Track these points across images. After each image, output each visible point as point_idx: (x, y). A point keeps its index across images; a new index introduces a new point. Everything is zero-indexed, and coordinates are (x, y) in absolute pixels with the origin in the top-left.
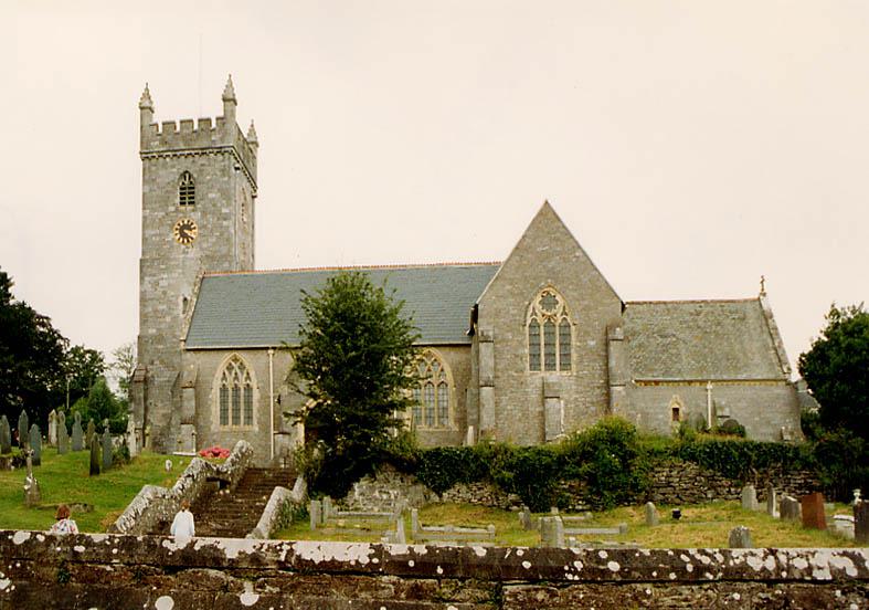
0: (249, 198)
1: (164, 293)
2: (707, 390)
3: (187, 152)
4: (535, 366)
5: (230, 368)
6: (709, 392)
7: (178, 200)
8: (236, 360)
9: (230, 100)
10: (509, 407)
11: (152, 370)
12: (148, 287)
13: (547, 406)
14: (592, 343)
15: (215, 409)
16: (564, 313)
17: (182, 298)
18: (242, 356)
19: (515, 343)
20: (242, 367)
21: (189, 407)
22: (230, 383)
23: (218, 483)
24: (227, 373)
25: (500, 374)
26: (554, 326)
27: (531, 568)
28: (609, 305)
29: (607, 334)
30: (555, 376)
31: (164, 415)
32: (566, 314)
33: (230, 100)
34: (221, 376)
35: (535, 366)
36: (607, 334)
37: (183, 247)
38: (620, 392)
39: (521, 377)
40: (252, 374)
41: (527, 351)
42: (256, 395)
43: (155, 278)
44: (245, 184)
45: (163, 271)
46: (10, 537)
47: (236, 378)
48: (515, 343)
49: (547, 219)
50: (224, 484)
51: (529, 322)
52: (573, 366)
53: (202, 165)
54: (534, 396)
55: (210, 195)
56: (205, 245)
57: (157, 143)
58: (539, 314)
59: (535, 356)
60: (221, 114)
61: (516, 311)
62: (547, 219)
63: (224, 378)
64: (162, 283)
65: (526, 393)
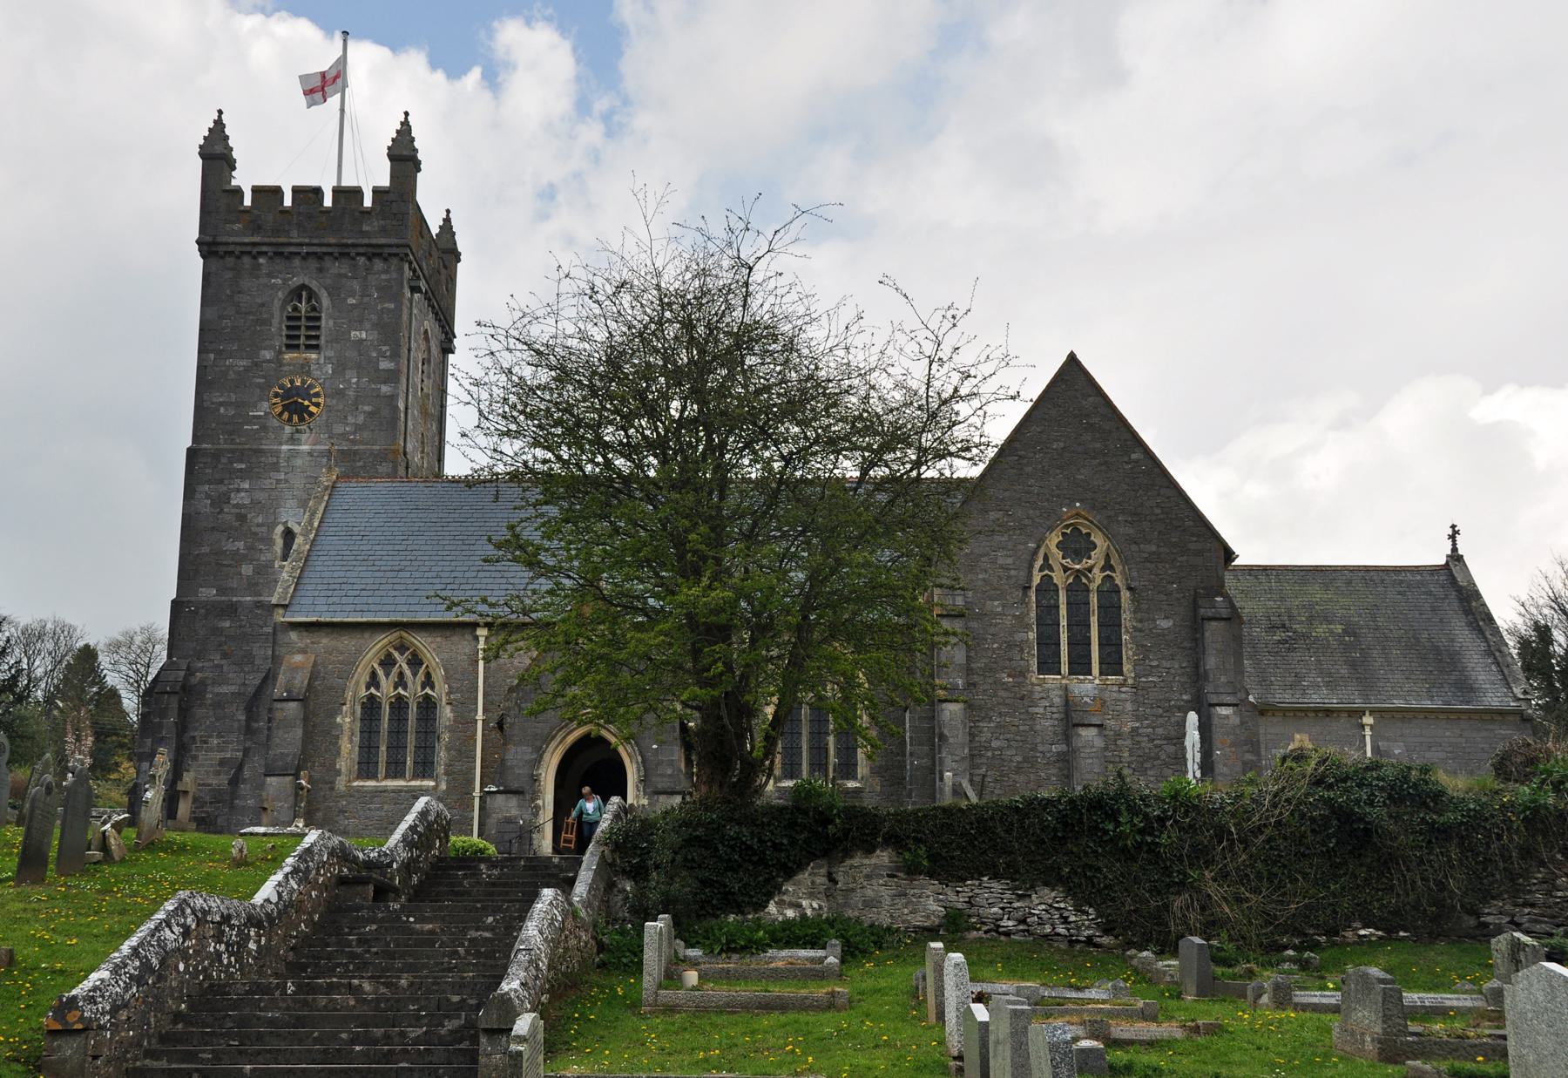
0: (435, 351)
1: (242, 518)
2: (1363, 727)
3: (305, 249)
4: (1048, 664)
5: (388, 662)
6: (1368, 732)
7: (280, 341)
8: (402, 648)
9: (404, 156)
10: (995, 744)
11: (201, 670)
12: (205, 506)
13: (1077, 742)
14: (1165, 624)
15: (348, 748)
16: (1108, 566)
17: (280, 529)
18: (420, 641)
19: (1008, 621)
20: (415, 662)
21: (289, 740)
22: (387, 689)
23: (371, 887)
24: (380, 672)
25: (976, 678)
26: (1088, 590)
27: (346, 300)
28: (1199, 553)
29: (1195, 606)
30: (1087, 687)
31: (222, 762)
32: (1112, 569)
33: (404, 156)
34: (366, 678)
35: (1048, 664)
36: (1195, 606)
37: (288, 429)
38: (1227, 717)
39: (1019, 685)
40: (438, 675)
41: (1032, 635)
42: (446, 713)
43: (223, 488)
44: (429, 324)
45: (243, 475)
46: (65, 1000)
47: (401, 682)
48: (1008, 621)
49: (1072, 358)
50: (383, 892)
51: (1036, 580)
52: (1127, 667)
53: (341, 276)
54: (1048, 724)
55: (354, 334)
56: (339, 429)
57: (237, 226)
58: (1056, 567)
59: (1048, 642)
60: (385, 181)
61: (1010, 561)
62: (1072, 358)
63: (374, 681)
64: (236, 499)
65: (1033, 717)
